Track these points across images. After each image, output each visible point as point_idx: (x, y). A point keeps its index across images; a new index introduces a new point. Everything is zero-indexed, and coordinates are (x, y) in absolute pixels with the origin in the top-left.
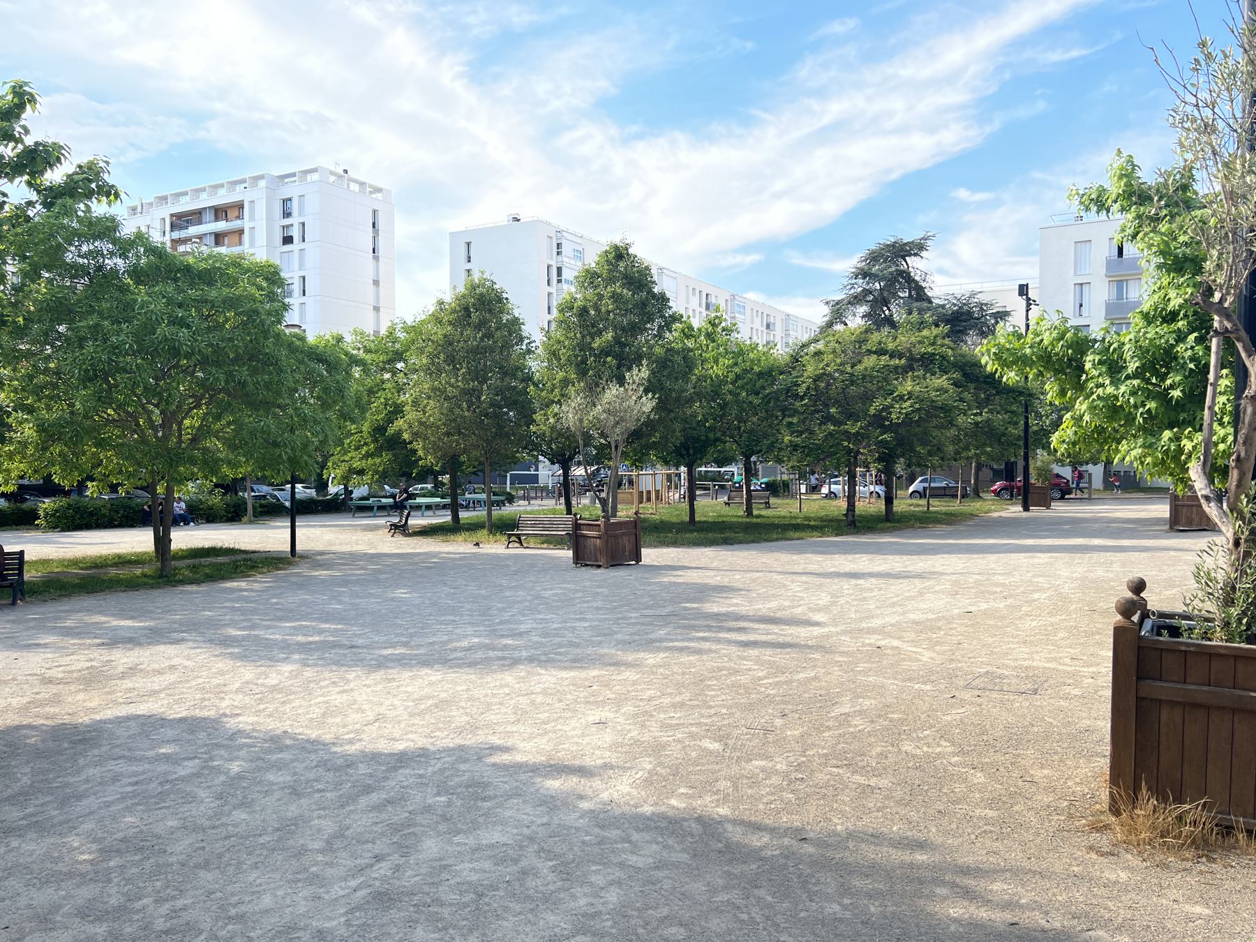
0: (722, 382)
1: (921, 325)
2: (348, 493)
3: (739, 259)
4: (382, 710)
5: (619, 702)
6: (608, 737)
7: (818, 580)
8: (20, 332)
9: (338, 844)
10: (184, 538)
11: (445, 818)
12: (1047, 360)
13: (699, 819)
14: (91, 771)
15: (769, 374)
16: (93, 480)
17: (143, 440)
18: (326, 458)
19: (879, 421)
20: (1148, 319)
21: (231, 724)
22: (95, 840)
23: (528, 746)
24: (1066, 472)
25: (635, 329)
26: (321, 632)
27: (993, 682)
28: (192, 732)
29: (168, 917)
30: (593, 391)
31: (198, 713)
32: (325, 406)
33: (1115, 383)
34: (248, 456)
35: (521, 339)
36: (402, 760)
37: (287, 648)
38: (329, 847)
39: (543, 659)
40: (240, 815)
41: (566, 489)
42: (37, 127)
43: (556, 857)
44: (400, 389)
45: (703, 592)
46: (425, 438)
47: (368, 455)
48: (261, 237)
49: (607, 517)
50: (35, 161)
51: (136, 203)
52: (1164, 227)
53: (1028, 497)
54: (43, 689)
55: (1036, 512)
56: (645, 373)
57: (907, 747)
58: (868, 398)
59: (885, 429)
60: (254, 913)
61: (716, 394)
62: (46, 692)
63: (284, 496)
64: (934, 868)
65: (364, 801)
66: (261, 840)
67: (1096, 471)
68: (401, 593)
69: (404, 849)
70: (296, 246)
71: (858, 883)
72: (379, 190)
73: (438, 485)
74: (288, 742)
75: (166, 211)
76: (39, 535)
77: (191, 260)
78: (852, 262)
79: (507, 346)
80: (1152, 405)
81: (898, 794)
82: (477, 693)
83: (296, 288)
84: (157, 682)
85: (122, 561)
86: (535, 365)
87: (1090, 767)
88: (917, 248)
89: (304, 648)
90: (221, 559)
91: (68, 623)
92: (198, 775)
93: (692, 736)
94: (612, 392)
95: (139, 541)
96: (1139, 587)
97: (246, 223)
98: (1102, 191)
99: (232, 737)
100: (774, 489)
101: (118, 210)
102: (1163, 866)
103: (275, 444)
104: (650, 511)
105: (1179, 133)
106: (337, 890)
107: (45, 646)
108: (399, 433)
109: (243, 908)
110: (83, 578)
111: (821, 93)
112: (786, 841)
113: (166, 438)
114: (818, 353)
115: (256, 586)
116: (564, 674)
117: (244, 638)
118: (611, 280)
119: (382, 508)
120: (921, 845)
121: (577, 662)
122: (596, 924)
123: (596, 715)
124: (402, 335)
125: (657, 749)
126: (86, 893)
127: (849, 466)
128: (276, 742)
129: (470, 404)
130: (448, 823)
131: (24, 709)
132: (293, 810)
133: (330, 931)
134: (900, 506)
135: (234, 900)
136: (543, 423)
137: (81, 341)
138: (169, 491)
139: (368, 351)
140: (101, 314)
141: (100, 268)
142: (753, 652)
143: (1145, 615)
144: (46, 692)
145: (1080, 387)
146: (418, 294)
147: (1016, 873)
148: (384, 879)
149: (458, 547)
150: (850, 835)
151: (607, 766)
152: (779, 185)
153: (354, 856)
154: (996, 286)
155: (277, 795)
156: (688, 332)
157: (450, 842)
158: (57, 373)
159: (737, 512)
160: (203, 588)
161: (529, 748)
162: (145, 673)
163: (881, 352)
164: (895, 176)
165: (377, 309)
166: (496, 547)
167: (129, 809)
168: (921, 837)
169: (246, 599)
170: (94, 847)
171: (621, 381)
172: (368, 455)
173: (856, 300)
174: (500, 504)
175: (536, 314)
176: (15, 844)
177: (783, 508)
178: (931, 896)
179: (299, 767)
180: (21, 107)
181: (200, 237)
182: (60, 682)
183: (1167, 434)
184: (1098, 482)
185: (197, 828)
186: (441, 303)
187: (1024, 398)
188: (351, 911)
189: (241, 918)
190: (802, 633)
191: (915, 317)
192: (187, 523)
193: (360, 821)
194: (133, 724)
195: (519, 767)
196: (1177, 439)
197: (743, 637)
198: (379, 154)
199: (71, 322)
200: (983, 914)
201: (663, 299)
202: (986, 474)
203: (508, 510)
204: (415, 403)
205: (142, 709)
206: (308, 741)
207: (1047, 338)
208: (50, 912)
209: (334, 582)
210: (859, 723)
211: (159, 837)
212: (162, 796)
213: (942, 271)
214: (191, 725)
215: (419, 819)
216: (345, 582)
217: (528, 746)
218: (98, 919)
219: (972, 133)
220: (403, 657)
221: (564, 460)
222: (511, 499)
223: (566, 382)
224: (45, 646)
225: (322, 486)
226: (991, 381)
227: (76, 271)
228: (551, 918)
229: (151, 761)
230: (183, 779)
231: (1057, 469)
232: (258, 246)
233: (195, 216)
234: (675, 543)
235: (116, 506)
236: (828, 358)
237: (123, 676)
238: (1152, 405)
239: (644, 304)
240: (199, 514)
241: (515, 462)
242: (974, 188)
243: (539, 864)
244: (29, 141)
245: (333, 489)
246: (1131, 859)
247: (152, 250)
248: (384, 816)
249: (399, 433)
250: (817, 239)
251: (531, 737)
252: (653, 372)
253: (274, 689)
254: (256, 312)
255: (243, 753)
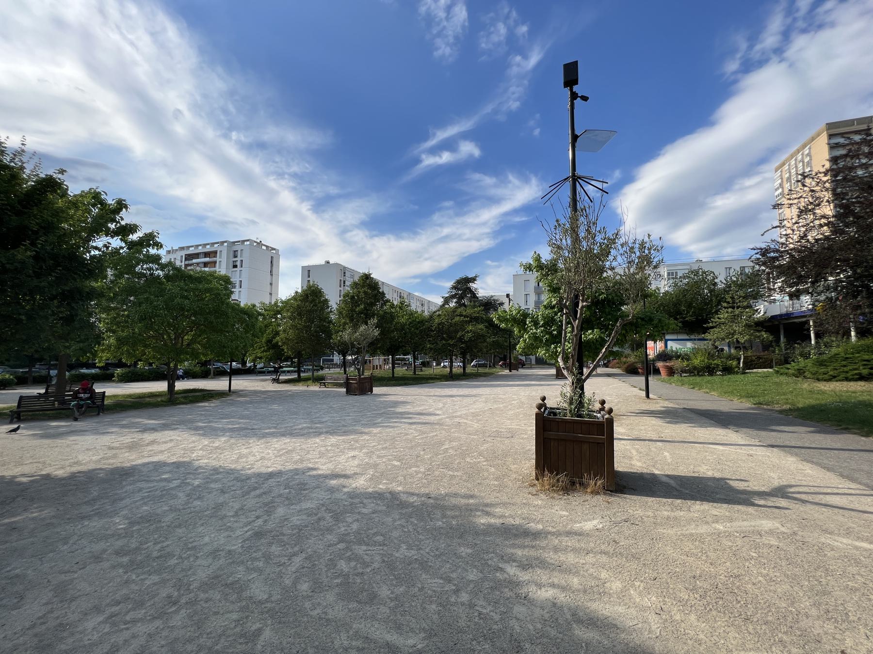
0: (405, 324)
1: (474, 307)
2: (255, 366)
3: (412, 280)
4: (263, 455)
5: (361, 448)
6: (356, 462)
7: (439, 398)
8: (111, 300)
9: (240, 513)
10: (180, 385)
11: (287, 498)
12: (514, 320)
13: (390, 493)
14: (128, 488)
15: (422, 322)
16: (141, 360)
17: (165, 344)
18: (246, 352)
19: (461, 340)
20: (546, 307)
21: (196, 464)
22: (127, 519)
23: (324, 467)
24: (523, 358)
25: (373, 304)
26: (239, 424)
27: (497, 434)
28: (178, 468)
29: (159, 551)
30: (356, 327)
31: (181, 460)
32: (246, 332)
33: (536, 329)
34: (212, 351)
35: (328, 307)
36: (271, 475)
37: (224, 430)
38: (236, 514)
39: (332, 432)
40: (197, 503)
41: (344, 364)
42: (126, 218)
43: (333, 511)
44: (279, 325)
45: (396, 404)
46: (288, 345)
47: (264, 351)
48: (224, 265)
49: (360, 376)
50: (125, 231)
51: (170, 249)
52: (549, 278)
53: (511, 367)
54: (109, 452)
55: (514, 372)
56: (376, 321)
57: (468, 460)
58: (457, 332)
59: (463, 343)
60: (200, 545)
61: (403, 329)
62: (110, 453)
63: (227, 368)
64: (476, 505)
65: (253, 494)
66: (206, 513)
67: (533, 358)
68: (275, 407)
69: (269, 513)
70: (238, 269)
71: (449, 513)
72: (274, 249)
73: (293, 362)
74: (221, 470)
75: (183, 253)
76: (114, 384)
77: (192, 273)
78: (449, 284)
79: (322, 309)
80: (547, 336)
81: (464, 478)
82: (303, 446)
83: (237, 285)
84: (164, 447)
85: (152, 395)
86: (333, 317)
87: (529, 464)
88: (473, 280)
89: (232, 430)
90: (197, 394)
91: (124, 422)
92: (179, 486)
93: (389, 460)
94: (363, 328)
95: (161, 386)
96: (544, 399)
97: (218, 259)
98: (530, 264)
99: (196, 469)
100: (425, 364)
101: (162, 252)
102: (553, 498)
103: (224, 347)
104: (378, 373)
105: (550, 249)
106: (238, 533)
107: (112, 433)
108: (277, 343)
109: (195, 544)
110: (133, 402)
111: (441, 225)
112: (423, 499)
113: (176, 344)
114: (439, 315)
115: (212, 405)
116: (340, 438)
117: (205, 427)
118: (363, 286)
119: (269, 372)
120: (472, 497)
121: (345, 433)
122: (348, 538)
123: (352, 453)
124: (280, 304)
125: (375, 466)
126: (120, 543)
127: (450, 356)
128: (216, 471)
129: (307, 331)
130: (289, 501)
131: (99, 461)
132: (221, 499)
133: (234, 551)
134: (468, 370)
135: (191, 540)
136: (336, 339)
137: (140, 304)
138: (176, 366)
139: (266, 310)
140: (150, 293)
141: (152, 274)
142: (414, 426)
143: (546, 408)
144: (110, 453)
145: (525, 330)
146: (289, 287)
147: (505, 504)
148: (260, 526)
149: (300, 388)
150: (446, 495)
151: (355, 474)
152: (427, 256)
153: (247, 517)
154: (500, 294)
155: (215, 493)
156: (392, 306)
157: (289, 509)
158: (128, 316)
159: (410, 373)
160: (189, 406)
161: (324, 468)
162: (159, 443)
163: (461, 315)
164: (466, 255)
165: (271, 294)
166: (315, 388)
167: (145, 504)
168: (472, 493)
169: (207, 410)
170: (127, 521)
171: (366, 324)
172: (264, 351)
173: (452, 297)
174: (318, 370)
175: (334, 298)
176: (86, 523)
177: (427, 371)
178: (474, 516)
179: (225, 481)
180: (121, 210)
181: (198, 264)
182: (117, 448)
183: (553, 346)
184: (533, 362)
185: (176, 510)
186: (296, 292)
187: (509, 332)
188: (244, 541)
189: (194, 548)
190: (432, 419)
191: (472, 303)
192: (183, 379)
193: (251, 502)
194: (150, 465)
195: (320, 475)
196: (556, 348)
197: (410, 421)
198: (273, 236)
199: (136, 296)
200: (493, 521)
201: (383, 294)
202: (497, 359)
203: (321, 373)
204: (284, 331)
205: (155, 459)
206: (231, 470)
207: (514, 313)
208: (101, 554)
209: (246, 402)
210: (451, 452)
211: (158, 515)
212: (162, 496)
213: (482, 288)
214: (178, 465)
215: (276, 500)
216: (251, 402)
217: (324, 467)
218: (125, 555)
219: (492, 242)
220: (274, 433)
221: (344, 353)
222: (322, 368)
223: (345, 324)
224: (112, 433)
225: (244, 363)
226: (497, 327)
227: (141, 275)
228: (329, 537)
229: (158, 481)
230: (172, 489)
231: (520, 357)
232: (222, 269)
233: (197, 256)
234: (386, 385)
235: (151, 372)
236: (443, 317)
237: (148, 445)
238: (547, 336)
239: (376, 295)
240: (189, 375)
241: (324, 354)
242: (493, 261)
243: (325, 515)
244: (123, 223)
245: (248, 365)
246: (542, 496)
247: (178, 270)
248: (261, 499)
249: (277, 343)
250: (440, 275)
251: (325, 464)
252: (379, 321)
253: (217, 448)
254: (219, 294)
255: (200, 476)
